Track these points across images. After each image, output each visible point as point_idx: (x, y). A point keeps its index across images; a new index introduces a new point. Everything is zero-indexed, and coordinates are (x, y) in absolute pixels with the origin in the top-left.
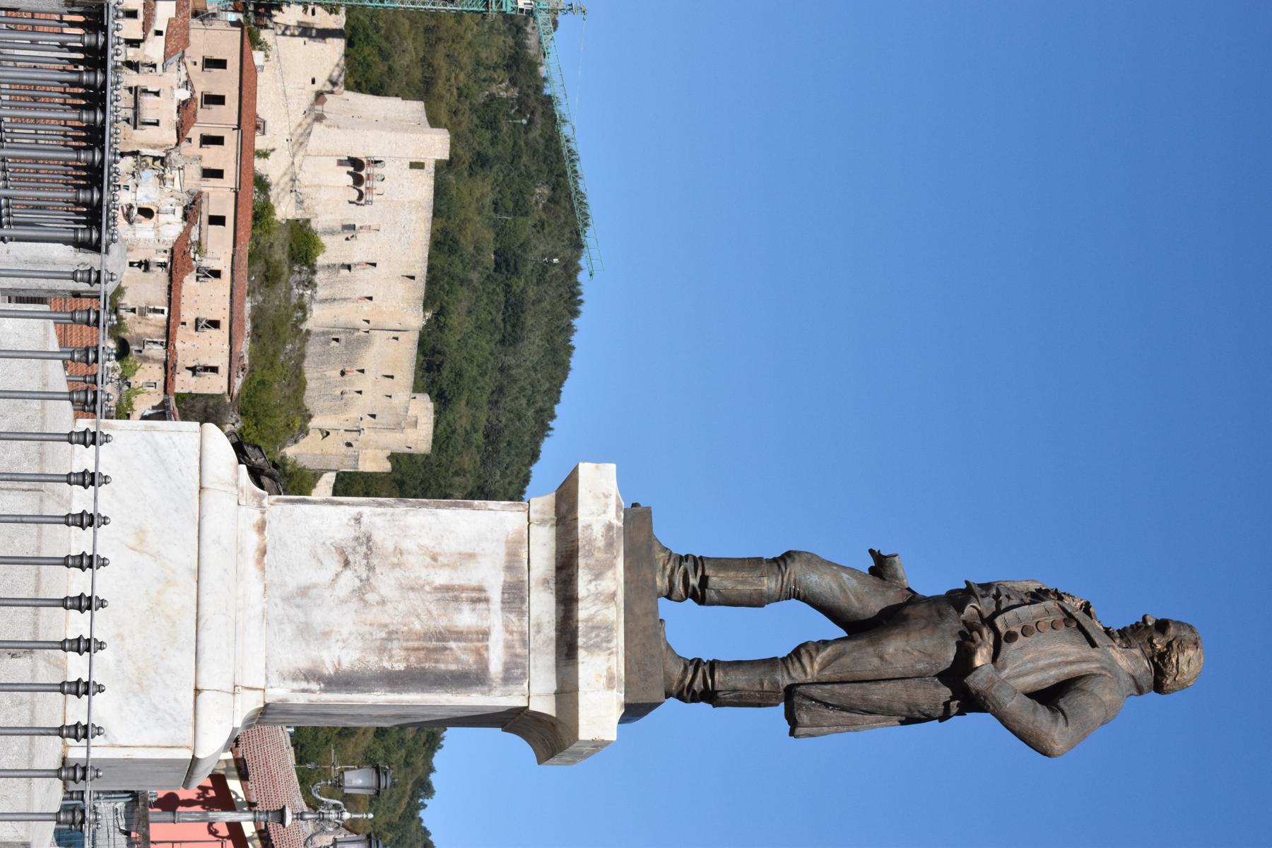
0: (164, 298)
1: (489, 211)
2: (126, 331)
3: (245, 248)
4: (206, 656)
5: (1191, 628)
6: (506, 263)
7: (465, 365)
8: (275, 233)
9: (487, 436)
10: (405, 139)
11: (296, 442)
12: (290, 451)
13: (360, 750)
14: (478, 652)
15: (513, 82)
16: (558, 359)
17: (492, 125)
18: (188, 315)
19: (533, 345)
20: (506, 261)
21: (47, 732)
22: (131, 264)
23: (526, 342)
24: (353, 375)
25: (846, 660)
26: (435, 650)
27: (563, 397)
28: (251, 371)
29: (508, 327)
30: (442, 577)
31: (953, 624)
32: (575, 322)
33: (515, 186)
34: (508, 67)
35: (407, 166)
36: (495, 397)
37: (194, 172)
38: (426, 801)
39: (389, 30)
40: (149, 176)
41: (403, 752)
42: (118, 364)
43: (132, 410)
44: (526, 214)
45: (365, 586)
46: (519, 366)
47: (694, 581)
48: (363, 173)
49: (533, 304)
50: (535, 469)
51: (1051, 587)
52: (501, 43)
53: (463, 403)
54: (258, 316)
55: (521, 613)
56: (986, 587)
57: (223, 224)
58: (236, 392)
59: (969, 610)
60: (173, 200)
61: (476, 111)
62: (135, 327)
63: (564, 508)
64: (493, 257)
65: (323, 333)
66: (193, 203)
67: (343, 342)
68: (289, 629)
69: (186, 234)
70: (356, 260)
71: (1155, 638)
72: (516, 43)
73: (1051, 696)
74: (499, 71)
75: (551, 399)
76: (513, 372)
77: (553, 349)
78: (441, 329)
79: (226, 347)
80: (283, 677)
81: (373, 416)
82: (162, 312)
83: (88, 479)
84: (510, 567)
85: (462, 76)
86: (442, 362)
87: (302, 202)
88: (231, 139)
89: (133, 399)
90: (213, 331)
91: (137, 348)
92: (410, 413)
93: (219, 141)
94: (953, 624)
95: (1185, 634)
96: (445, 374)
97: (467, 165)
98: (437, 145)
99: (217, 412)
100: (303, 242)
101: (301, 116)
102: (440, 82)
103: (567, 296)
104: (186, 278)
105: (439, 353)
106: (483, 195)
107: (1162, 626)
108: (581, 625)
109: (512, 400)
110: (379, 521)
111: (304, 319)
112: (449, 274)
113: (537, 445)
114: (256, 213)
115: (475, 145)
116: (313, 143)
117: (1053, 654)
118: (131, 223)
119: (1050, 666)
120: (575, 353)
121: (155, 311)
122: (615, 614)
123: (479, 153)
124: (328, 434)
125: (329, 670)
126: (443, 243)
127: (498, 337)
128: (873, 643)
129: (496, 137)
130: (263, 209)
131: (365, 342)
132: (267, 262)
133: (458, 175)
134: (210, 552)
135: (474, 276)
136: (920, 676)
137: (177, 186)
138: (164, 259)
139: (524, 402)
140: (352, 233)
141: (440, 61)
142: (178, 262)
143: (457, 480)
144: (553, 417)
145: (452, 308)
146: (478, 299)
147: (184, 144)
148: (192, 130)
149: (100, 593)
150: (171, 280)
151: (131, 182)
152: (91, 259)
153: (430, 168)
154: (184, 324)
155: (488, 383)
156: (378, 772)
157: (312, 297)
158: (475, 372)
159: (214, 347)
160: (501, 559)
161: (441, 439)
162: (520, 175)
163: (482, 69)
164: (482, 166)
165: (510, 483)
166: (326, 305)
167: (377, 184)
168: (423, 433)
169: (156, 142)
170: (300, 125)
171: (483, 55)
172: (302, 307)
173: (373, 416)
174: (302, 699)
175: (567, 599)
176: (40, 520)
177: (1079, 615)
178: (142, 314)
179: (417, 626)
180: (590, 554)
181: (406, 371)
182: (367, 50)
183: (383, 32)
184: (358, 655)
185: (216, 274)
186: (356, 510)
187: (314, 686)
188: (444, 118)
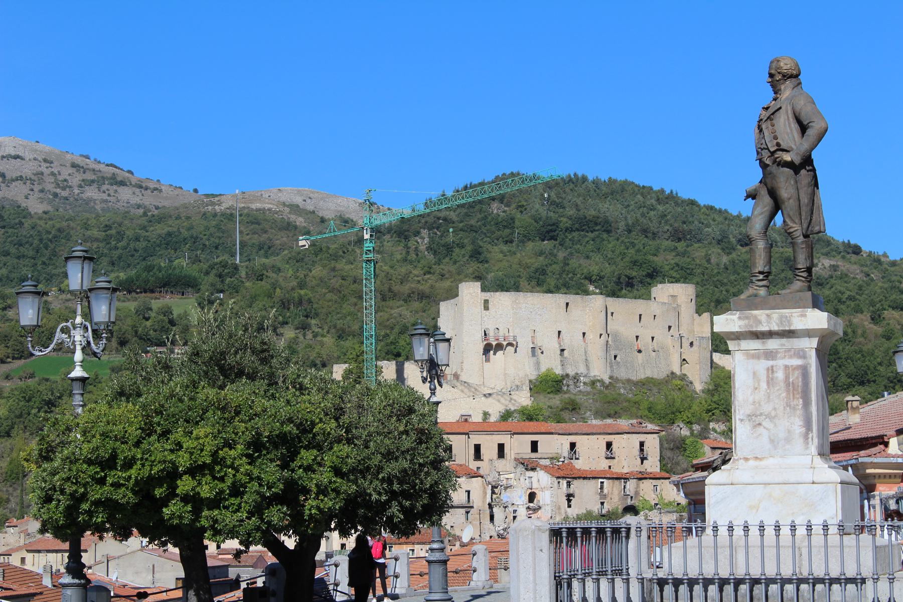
0: (593, 481)
2: (617, 508)
3: (552, 426)
4: (800, 480)
5: (771, 62)
6: (549, 232)
7: (627, 259)
8: (541, 405)
9: (679, 240)
10: (468, 313)
11: (691, 383)
12: (698, 387)
15: (417, 233)
16: (618, 190)
17: (449, 248)
18: (604, 464)
19: (610, 209)
20: (548, 232)
21: (826, 540)
22: (569, 506)
23: (608, 214)
24: (641, 344)
25: (791, 213)
26: (793, 387)
27: (647, 184)
28: (641, 417)
29: (597, 228)
30: (764, 385)
31: (774, 169)
32: (590, 178)
34: (407, 238)
35: (487, 313)
36: (650, 235)
37: (500, 464)
39: (385, 327)
40: (505, 496)
42: (642, 513)
43: (674, 502)
44: (513, 219)
45: (768, 416)
46: (626, 218)
47: (761, 277)
48: (494, 343)
49: (579, 210)
50: (702, 202)
51: (756, 123)
52: (389, 244)
53: (655, 258)
54: (601, 414)
55: (777, 352)
56: (758, 153)
57: (537, 442)
58: (657, 428)
59: (768, 162)
60: (522, 479)
61: (440, 260)
62: (614, 502)
63: (733, 337)
64: (546, 242)
65: (611, 367)
66: (523, 464)
67: (617, 352)
68: (787, 447)
69: (545, 468)
70: (557, 346)
71: (780, 78)
72: (389, 232)
73: (803, 128)
74: (409, 245)
75: (649, 193)
76: (630, 222)
78: (601, 278)
79: (625, 436)
80: (807, 448)
81: (670, 327)
82: (602, 483)
83: (731, 528)
84: (759, 358)
85: (416, 272)
86: (626, 276)
87: (517, 386)
88: (475, 439)
89: (666, 501)
90: (614, 446)
91: (629, 500)
92: (666, 301)
93: (477, 448)
94: (774, 169)
95: (774, 65)
96: (634, 274)
97: (480, 265)
98: (470, 291)
99: (673, 441)
100: (548, 385)
101: (455, 390)
102: (421, 288)
103: (572, 186)
104: (577, 467)
105: (619, 278)
106: (502, 252)
107: (771, 75)
108: (781, 329)
109: (651, 221)
110: (742, 412)
111: (602, 381)
114: (527, 419)
115: (465, 259)
116: (474, 380)
117: (785, 125)
118: (540, 508)
119: (790, 127)
120: (614, 177)
121: (602, 488)
122: (776, 314)
123: (471, 257)
124: (684, 360)
126: (539, 280)
127: (605, 236)
128: (783, 202)
129: (458, 245)
130: (524, 414)
131: (616, 336)
132: (562, 410)
133: (488, 271)
134: (758, 479)
135: (561, 255)
136: (796, 182)
137: (512, 476)
138: (564, 483)
139: (652, 213)
140: (537, 349)
141: (406, 288)
142: (566, 474)
143: (714, 260)
144: (662, 191)
146: (578, 251)
147: (481, 472)
148: (471, 467)
149: (773, 523)
150: (579, 478)
151: (511, 509)
152: (633, 532)
153: (487, 295)
154: (610, 467)
155: (640, 241)
156: (897, 352)
157: (585, 376)
158: (632, 251)
159: (625, 445)
160: (755, 361)
161: (683, 275)
162: (484, 225)
163: (409, 258)
164: (480, 254)
165: (714, 220)
166: (591, 365)
167: (501, 333)
168: (681, 290)
169: (481, 492)
170: (462, 391)
172: (593, 383)
173: (670, 327)
174: (816, 440)
175: (770, 334)
176: (747, 546)
177: (768, 114)
178: (605, 496)
179: (784, 395)
180: (751, 326)
181: (638, 306)
183: (388, 332)
184: (797, 419)
185: (573, 445)
186: (738, 421)
187: (810, 436)
188: (447, 284)
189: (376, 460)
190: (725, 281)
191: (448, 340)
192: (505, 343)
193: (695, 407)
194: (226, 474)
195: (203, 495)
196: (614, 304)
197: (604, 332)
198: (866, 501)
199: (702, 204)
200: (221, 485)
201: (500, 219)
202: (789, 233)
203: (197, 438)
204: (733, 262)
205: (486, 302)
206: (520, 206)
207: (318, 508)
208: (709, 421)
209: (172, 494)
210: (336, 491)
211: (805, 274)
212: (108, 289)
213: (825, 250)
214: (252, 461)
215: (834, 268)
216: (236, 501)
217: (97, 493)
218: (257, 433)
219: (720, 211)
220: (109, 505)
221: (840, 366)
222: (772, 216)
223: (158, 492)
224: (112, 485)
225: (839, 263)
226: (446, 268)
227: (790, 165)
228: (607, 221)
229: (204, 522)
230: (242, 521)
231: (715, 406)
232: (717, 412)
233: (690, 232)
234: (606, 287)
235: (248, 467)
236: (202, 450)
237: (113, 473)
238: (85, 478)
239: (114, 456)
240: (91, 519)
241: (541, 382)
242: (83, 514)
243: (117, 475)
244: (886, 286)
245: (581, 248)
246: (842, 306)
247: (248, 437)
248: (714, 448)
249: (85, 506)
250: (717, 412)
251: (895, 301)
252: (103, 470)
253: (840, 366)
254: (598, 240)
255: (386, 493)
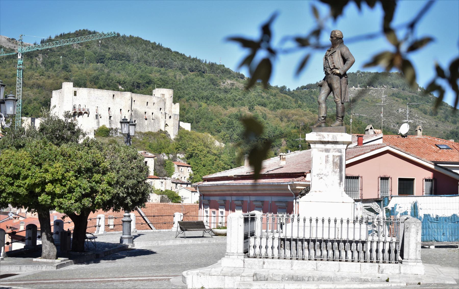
1: (83, 65)
6: (101, 59)
7: (138, 74)
9: (162, 67)
11: (169, 135)
12: (172, 137)
13: (270, 112)
14: (336, 157)
15: (37, 56)
17: (52, 64)
19: (130, 50)
20: (100, 59)
21: (354, 226)
23: (129, 53)
25: (337, 94)
27: (148, 39)
28: (146, 150)
29: (123, 59)
32: (121, 35)
33: (74, 56)
34: (31, 57)
36: (148, 64)
38: (287, 89)
41: (271, 97)
47: (323, 118)
50: (173, 50)
55: (330, 150)
59: (329, 72)
64: (99, 64)
67: (136, 119)
73: (345, 61)
77: (131, 43)
78: (125, 83)
81: (161, 109)
84: (323, 151)
94: (332, 76)
96: (140, 82)
98: (68, 87)
99: (160, 161)
105: (133, 83)
106: (78, 67)
112: (106, 80)
113: (164, 49)
115: (60, 70)
120: (132, 35)
122: (331, 134)
123: (63, 69)
125: (339, 181)
127: (127, 63)
128: (335, 89)
129: (56, 62)
131: (136, 111)
135: (106, 71)
139: (150, 53)
140: (98, 116)
143: (178, 78)
144: (155, 43)
145: (117, 79)
153: (76, 89)
155: (143, 66)
158: (139, 71)
160: (321, 152)
161: (164, 84)
164: (67, 67)
165: (178, 59)
167: (82, 107)
171: (28, 66)
173: (161, 109)
175: (328, 142)
181: (147, 98)
182: (29, 108)
189: (123, 179)
190: (183, 87)
191: (135, 125)
192: (83, 112)
193: (171, 147)
194: (67, 184)
195: (57, 192)
196: (136, 97)
197: (130, 109)
198: (294, 200)
199: (173, 51)
200: (65, 188)
201: (77, 52)
202: (336, 102)
203: (56, 168)
204: (186, 79)
205: (75, 92)
206: (87, 46)
207: (102, 199)
208: (177, 153)
209: (43, 191)
210: (109, 192)
211: (341, 119)
212: (14, 100)
213: (229, 76)
214: (77, 178)
215: (233, 85)
216: (70, 195)
217: (10, 189)
218: (80, 167)
219: (181, 54)
220: (15, 195)
221: (234, 130)
222: (329, 94)
223: (37, 190)
224: (17, 186)
225: (235, 83)
226: (51, 73)
227: (339, 75)
228: (128, 56)
229: (55, 204)
230: (72, 204)
231: (180, 146)
232: (180, 149)
233: (167, 63)
234: (127, 87)
235: (75, 181)
236: (57, 173)
237: (18, 181)
238: (4, 182)
239: (19, 174)
240: (6, 200)
241: (100, 131)
242: (2, 198)
243: (19, 182)
244: (256, 94)
245: (116, 68)
246: (236, 103)
247: (76, 168)
248: (179, 166)
249: (4, 195)
250: (180, 149)
251: (259, 101)
252: (13, 179)
253: (234, 130)
254: (124, 65)
255: (126, 193)
